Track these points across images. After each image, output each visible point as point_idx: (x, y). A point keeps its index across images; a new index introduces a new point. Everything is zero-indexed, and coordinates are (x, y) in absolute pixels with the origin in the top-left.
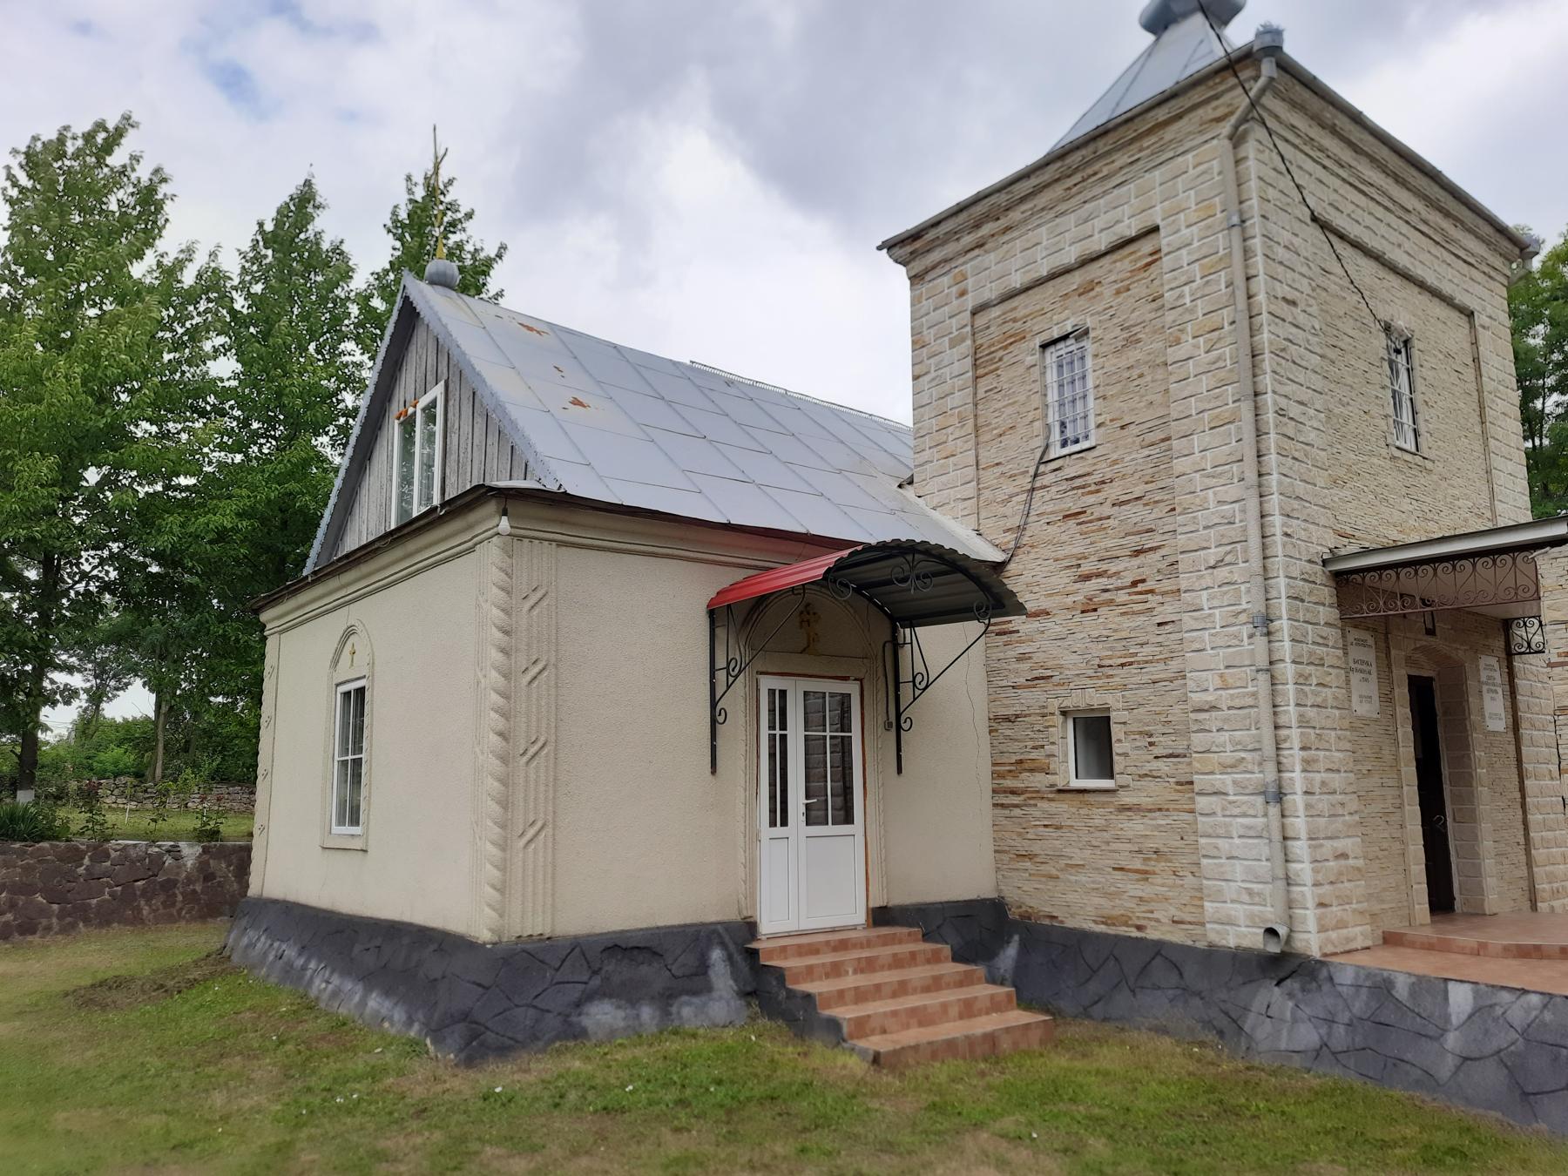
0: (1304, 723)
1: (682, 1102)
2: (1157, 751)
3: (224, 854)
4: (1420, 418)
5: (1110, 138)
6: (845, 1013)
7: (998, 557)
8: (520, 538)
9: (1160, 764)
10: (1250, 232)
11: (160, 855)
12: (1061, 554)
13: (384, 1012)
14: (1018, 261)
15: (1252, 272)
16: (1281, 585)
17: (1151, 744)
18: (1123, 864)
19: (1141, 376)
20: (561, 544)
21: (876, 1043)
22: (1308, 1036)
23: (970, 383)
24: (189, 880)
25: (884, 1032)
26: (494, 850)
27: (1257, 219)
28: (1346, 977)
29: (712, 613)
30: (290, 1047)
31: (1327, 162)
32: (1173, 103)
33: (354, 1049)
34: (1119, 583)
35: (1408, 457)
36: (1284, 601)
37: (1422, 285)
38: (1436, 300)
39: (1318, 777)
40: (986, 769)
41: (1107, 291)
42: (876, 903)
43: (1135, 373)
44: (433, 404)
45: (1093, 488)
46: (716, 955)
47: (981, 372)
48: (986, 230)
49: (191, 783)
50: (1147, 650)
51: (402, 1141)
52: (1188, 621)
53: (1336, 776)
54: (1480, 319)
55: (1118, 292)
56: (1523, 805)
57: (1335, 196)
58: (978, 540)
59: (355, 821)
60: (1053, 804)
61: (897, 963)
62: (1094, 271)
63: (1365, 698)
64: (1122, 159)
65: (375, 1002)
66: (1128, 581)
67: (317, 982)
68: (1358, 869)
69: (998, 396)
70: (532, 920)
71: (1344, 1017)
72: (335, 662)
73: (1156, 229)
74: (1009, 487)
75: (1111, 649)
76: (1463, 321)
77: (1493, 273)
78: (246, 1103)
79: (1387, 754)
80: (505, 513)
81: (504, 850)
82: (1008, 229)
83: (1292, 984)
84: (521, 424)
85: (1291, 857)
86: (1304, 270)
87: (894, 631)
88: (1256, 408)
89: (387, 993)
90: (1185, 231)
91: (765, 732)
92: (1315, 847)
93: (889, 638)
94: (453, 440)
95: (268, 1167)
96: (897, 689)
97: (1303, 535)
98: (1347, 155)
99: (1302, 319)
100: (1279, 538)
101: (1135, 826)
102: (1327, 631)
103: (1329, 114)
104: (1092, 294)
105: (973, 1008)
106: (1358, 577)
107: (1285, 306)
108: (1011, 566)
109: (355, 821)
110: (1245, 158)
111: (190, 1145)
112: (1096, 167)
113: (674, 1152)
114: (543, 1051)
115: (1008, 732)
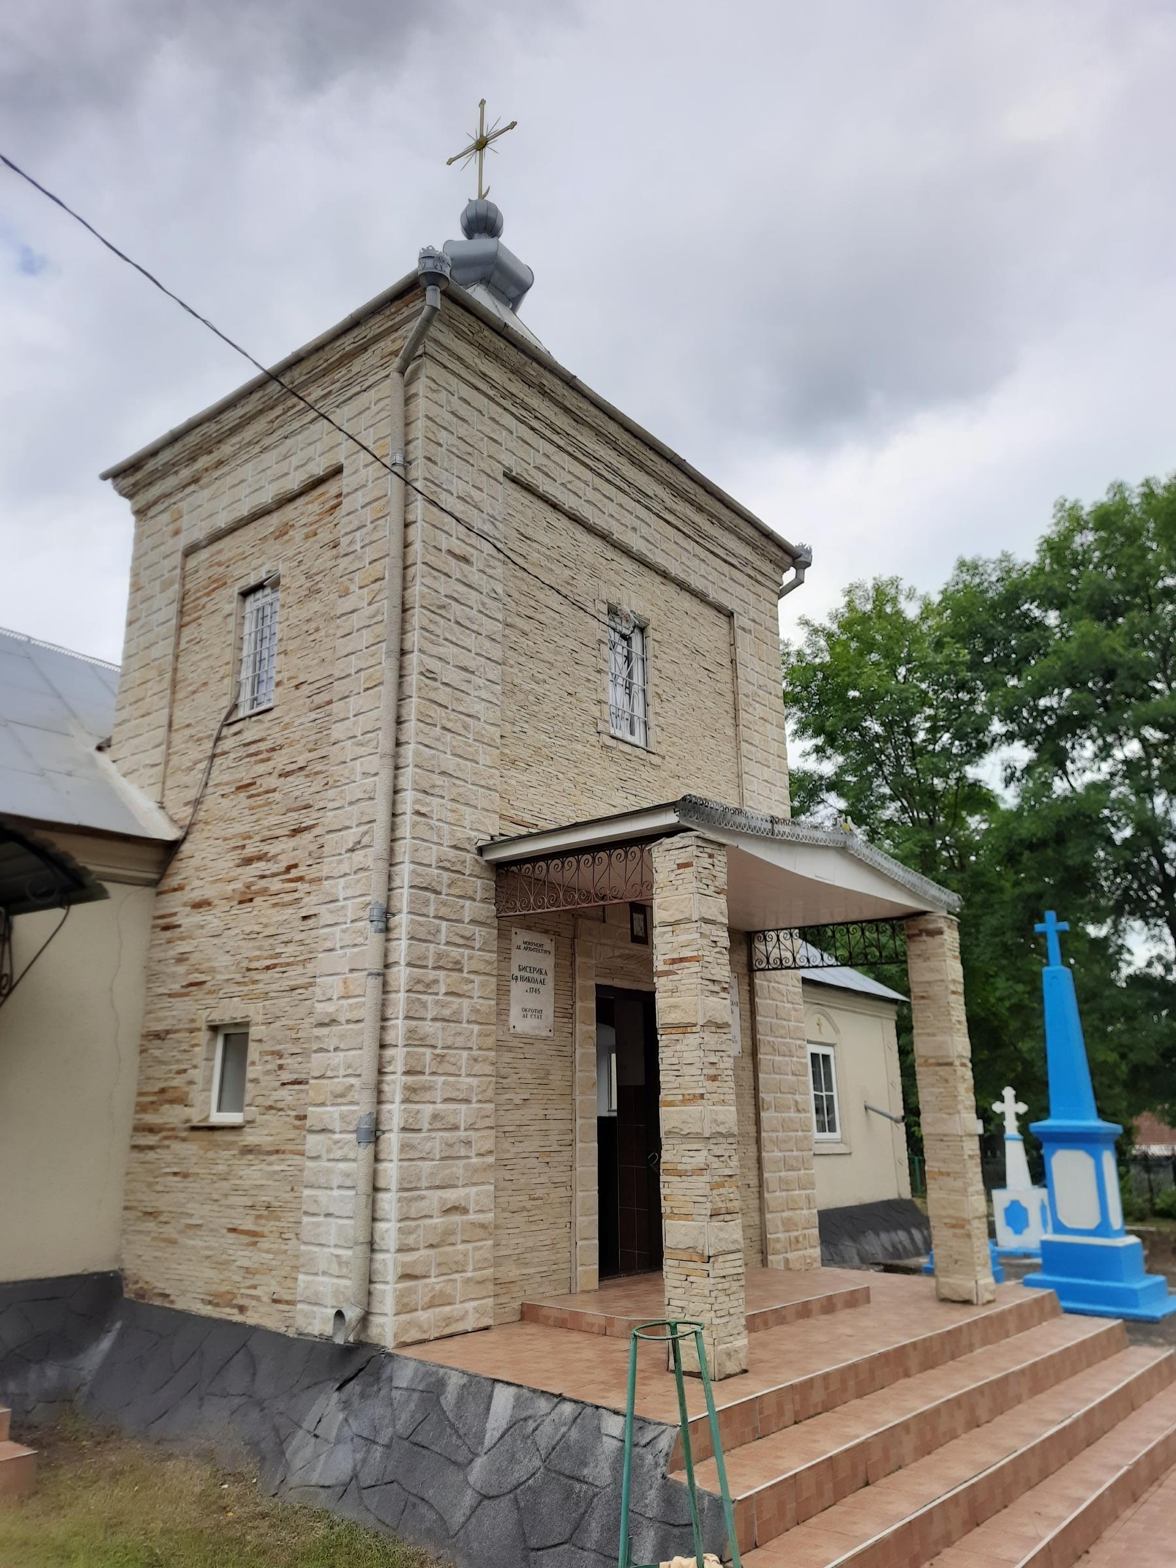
0: (414, 1039)
2: (286, 1076)
7: (169, 833)
9: (284, 1093)
14: (226, 500)
15: (411, 518)
16: (405, 873)
17: (281, 1067)
18: (236, 1223)
19: (317, 630)
22: (339, 1464)
23: (173, 632)
27: (421, 461)
28: (404, 1375)
32: (355, 332)
35: (638, 752)
36: (406, 892)
37: (665, 575)
39: (428, 1109)
41: (297, 534)
43: (313, 625)
45: (264, 756)
47: (186, 619)
48: (203, 462)
50: (290, 949)
52: (327, 918)
53: (463, 1107)
54: (739, 621)
55: (307, 537)
56: (758, 1141)
57: (545, 461)
60: (185, 1145)
62: (289, 513)
63: (531, 1011)
66: (284, 864)
68: (483, 1226)
69: (196, 648)
71: (384, 1437)
75: (260, 948)
76: (723, 621)
77: (759, 578)
79: (557, 1079)
82: (220, 463)
85: (379, 1215)
88: (401, 667)
90: (363, 472)
92: (410, 1200)
97: (451, 817)
98: (562, 421)
99: (475, 577)
101: (252, 1173)
103: (532, 370)
104: (286, 537)
106: (514, 868)
107: (453, 562)
108: (186, 848)
110: (415, 395)
115: (157, 1053)
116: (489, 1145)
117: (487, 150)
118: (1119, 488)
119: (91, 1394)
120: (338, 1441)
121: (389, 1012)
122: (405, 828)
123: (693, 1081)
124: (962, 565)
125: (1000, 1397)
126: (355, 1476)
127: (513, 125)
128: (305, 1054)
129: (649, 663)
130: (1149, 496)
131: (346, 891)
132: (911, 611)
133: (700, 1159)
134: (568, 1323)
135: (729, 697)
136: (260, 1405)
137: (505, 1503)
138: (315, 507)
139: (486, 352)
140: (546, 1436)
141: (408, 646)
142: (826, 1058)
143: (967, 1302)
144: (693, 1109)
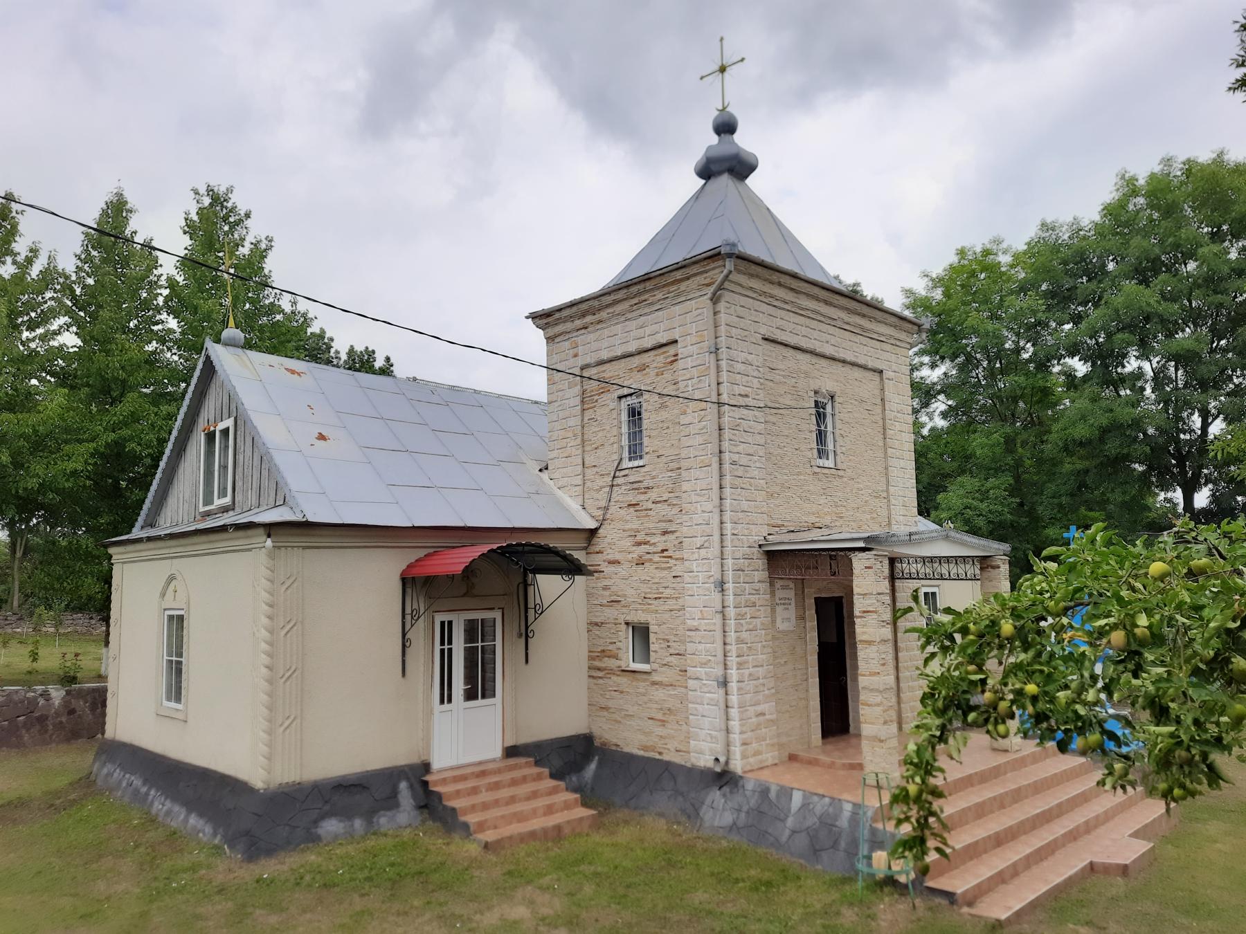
0: (740, 641)
1: (369, 879)
2: (672, 651)
3: (81, 694)
4: (838, 445)
5: (653, 282)
6: (472, 819)
7: (592, 525)
8: (279, 548)
10: (721, 357)
11: (35, 698)
12: (627, 527)
13: (199, 827)
16: (729, 563)
18: (653, 715)
20: (304, 548)
21: (490, 836)
22: (728, 818)
24: (57, 714)
25: (496, 827)
26: (264, 736)
28: (750, 786)
29: (404, 581)
30: (141, 850)
31: (776, 303)
33: (181, 851)
34: (655, 550)
36: (730, 572)
37: (844, 362)
38: (856, 368)
39: (747, 672)
40: (584, 653)
42: (509, 743)
44: (227, 429)
46: (403, 785)
47: (586, 406)
48: (589, 319)
49: (45, 616)
50: (668, 591)
51: (210, 908)
54: (886, 374)
55: (657, 375)
58: (583, 513)
59: (178, 699)
61: (514, 783)
62: (646, 358)
63: (786, 619)
64: (660, 296)
65: (193, 820)
66: (659, 549)
67: (156, 804)
70: (289, 772)
71: (745, 808)
72: (163, 595)
73: (676, 341)
74: (600, 482)
76: (876, 377)
78: (120, 888)
80: (269, 536)
81: (270, 734)
83: (726, 789)
84: (282, 468)
86: (755, 374)
87: (525, 575)
89: (201, 815)
91: (438, 647)
93: (521, 580)
94: (240, 458)
95: (136, 926)
96: (526, 612)
97: (746, 532)
98: (790, 296)
100: (729, 537)
101: (659, 694)
102: (757, 586)
103: (775, 277)
105: (555, 805)
108: (600, 531)
109: (178, 699)
111: (90, 915)
112: (646, 296)
113: (358, 908)
114: (294, 850)
116: (772, 685)
117: (726, 74)
118: (1168, 161)
119: (593, 789)
120: (724, 810)
121: (727, 629)
122: (728, 543)
123: (875, 666)
124: (1044, 226)
125: (1017, 796)
126: (734, 823)
127: (742, 60)
128: (683, 642)
129: (837, 417)
130: (1188, 172)
131: (698, 569)
132: (1005, 259)
133: (879, 699)
134: (812, 762)
135: (881, 423)
136: (682, 794)
137: (804, 834)
138: (661, 359)
139: (751, 276)
140: (819, 810)
141: (723, 449)
142: (934, 594)
143: (1006, 751)
144: (875, 678)
